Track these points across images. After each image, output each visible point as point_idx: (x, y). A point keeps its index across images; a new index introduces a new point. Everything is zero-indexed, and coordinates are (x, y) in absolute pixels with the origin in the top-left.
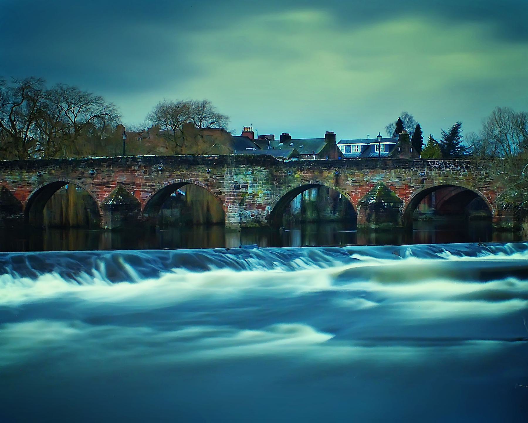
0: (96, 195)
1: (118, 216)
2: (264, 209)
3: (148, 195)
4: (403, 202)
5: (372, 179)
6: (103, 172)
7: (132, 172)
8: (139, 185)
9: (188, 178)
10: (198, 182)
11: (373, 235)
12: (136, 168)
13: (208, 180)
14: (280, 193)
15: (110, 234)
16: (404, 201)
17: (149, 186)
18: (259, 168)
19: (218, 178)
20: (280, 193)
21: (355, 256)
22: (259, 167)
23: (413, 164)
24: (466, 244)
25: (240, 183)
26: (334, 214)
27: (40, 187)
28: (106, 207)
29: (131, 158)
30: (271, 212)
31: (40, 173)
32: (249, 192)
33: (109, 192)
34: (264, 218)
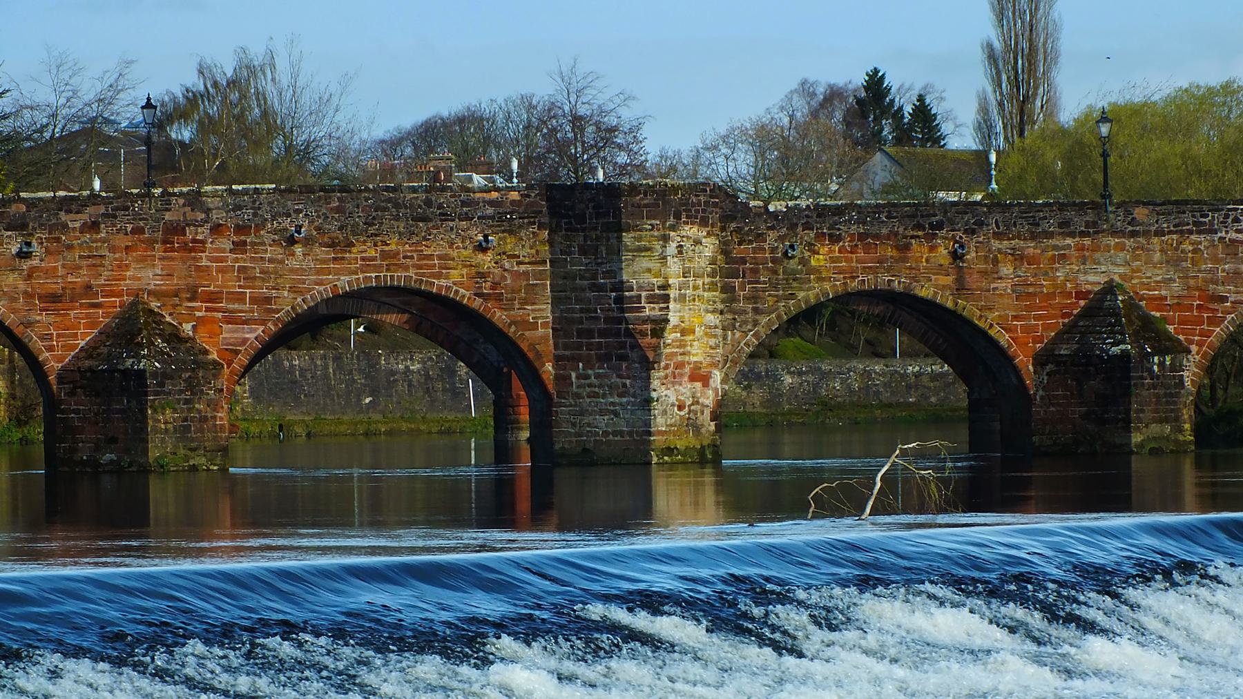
0: (42, 338)
2: (705, 380)
3: (252, 336)
4: (1189, 352)
5: (1085, 273)
6: (70, 247)
7: (185, 248)
8: (212, 298)
9: (406, 269)
10: (443, 282)
12: (203, 233)
13: (483, 275)
14: (756, 323)
16: (1194, 348)
17: (254, 300)
19: (523, 268)
20: (756, 323)
22: (695, 229)
23: (1227, 216)
25: (640, 288)
29: (181, 194)
31: (486, 237)
32: (673, 319)
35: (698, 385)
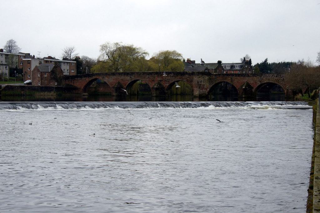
1: (158, 92)
11: (244, 99)
15: (155, 98)
18: (206, 76)
21: (249, 104)
24: (281, 102)
26: (220, 91)
27: (131, 81)
28: (153, 88)
30: (209, 91)
33: (154, 83)
34: (207, 93)
35: (205, 90)
